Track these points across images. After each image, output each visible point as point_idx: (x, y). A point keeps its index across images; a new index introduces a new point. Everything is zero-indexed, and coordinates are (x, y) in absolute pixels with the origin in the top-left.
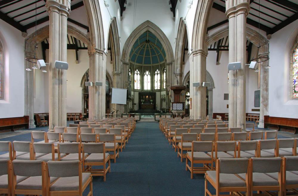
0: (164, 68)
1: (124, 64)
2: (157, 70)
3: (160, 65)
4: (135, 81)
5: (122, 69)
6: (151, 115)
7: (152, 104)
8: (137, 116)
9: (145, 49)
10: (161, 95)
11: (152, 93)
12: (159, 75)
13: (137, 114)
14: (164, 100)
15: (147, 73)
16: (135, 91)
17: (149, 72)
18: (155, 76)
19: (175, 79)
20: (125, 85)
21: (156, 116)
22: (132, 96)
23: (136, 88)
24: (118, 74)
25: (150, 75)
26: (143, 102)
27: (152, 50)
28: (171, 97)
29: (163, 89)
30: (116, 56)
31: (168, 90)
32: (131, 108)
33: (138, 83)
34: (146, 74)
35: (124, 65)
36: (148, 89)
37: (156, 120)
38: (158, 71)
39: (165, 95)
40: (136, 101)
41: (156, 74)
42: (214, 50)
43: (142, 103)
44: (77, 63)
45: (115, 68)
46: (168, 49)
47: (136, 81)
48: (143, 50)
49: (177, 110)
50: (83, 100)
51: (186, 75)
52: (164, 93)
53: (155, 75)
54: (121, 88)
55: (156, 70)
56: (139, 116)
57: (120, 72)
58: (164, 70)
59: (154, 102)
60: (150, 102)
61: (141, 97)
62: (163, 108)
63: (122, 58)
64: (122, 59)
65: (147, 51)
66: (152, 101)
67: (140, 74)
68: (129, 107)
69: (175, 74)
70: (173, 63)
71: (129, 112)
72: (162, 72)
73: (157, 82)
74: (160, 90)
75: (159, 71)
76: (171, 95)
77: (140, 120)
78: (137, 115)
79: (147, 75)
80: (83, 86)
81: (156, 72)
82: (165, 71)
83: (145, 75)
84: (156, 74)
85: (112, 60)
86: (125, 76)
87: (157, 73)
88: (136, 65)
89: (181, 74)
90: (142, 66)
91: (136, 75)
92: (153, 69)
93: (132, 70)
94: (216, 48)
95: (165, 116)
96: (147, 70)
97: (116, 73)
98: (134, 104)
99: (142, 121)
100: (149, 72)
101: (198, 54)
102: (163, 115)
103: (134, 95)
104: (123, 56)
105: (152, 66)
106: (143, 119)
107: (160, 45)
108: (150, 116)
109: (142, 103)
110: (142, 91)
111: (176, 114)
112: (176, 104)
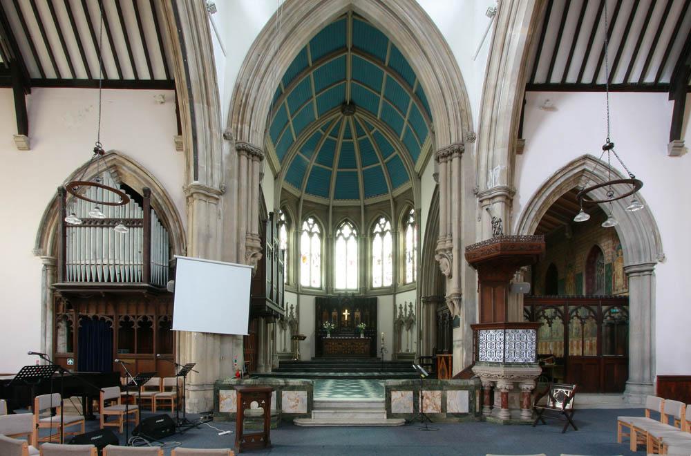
0: (409, 209)
1: (239, 150)
2: (382, 221)
3: (394, 199)
4: (304, 258)
5: (229, 175)
6: (363, 382)
7: (362, 336)
8: (292, 394)
9: (340, 141)
10: (398, 306)
11: (365, 303)
12: (388, 236)
13: (292, 382)
14: (410, 322)
15: (347, 229)
16: (300, 291)
17: (352, 229)
18: (374, 242)
19: (480, 218)
20: (243, 247)
21: (396, 395)
22: (292, 308)
23: (304, 282)
24: (208, 195)
25: (356, 238)
26: (333, 332)
27: (365, 145)
28: (460, 300)
29: (405, 284)
30: (197, 106)
31: (446, 272)
32: (289, 350)
33: (313, 267)
34: (341, 234)
35: (239, 156)
36: (385, 285)
37: (397, 416)
38: (385, 224)
39: (414, 304)
40: (307, 325)
41: (378, 235)
42: (656, 87)
43: (329, 336)
44: (20, 149)
45: (194, 167)
46: (443, 83)
47: (308, 257)
48: (330, 146)
49: (506, 364)
50: (50, 314)
51: (530, 204)
52: (409, 298)
53: (373, 235)
54: (224, 258)
55: (377, 221)
56: (303, 395)
57: (216, 187)
58: (406, 217)
59: (372, 331)
60: (358, 332)
61: (325, 314)
62: (404, 350)
63: (230, 124)
64: (231, 131)
65: (348, 149)
66: (362, 326)
67: (321, 235)
68: (278, 349)
69: (477, 194)
70: (467, 146)
71: (277, 365)
72: (400, 225)
73: (381, 261)
74: (393, 290)
75: (388, 223)
76: (460, 295)
77: (308, 415)
78: (293, 388)
79: (347, 239)
80: (48, 252)
81: (377, 229)
82: (412, 220)
83: (337, 238)
84: (378, 235)
85: (180, 132)
86: (244, 207)
87: (383, 229)
88: (304, 201)
89: (507, 189)
90: (328, 206)
91: (304, 238)
92: (365, 216)
93: (293, 220)
94: (666, 79)
95: (438, 393)
96: (346, 221)
97: (198, 187)
98: (297, 337)
99: (319, 418)
100: (354, 228)
101: (497, 199)
102: (431, 389)
103: (298, 307)
104: (235, 117)
105: (365, 206)
106: (326, 407)
107: (404, 72)
108: (362, 392)
109: (326, 333)
110: (327, 292)
111: (502, 385)
112: (501, 331)
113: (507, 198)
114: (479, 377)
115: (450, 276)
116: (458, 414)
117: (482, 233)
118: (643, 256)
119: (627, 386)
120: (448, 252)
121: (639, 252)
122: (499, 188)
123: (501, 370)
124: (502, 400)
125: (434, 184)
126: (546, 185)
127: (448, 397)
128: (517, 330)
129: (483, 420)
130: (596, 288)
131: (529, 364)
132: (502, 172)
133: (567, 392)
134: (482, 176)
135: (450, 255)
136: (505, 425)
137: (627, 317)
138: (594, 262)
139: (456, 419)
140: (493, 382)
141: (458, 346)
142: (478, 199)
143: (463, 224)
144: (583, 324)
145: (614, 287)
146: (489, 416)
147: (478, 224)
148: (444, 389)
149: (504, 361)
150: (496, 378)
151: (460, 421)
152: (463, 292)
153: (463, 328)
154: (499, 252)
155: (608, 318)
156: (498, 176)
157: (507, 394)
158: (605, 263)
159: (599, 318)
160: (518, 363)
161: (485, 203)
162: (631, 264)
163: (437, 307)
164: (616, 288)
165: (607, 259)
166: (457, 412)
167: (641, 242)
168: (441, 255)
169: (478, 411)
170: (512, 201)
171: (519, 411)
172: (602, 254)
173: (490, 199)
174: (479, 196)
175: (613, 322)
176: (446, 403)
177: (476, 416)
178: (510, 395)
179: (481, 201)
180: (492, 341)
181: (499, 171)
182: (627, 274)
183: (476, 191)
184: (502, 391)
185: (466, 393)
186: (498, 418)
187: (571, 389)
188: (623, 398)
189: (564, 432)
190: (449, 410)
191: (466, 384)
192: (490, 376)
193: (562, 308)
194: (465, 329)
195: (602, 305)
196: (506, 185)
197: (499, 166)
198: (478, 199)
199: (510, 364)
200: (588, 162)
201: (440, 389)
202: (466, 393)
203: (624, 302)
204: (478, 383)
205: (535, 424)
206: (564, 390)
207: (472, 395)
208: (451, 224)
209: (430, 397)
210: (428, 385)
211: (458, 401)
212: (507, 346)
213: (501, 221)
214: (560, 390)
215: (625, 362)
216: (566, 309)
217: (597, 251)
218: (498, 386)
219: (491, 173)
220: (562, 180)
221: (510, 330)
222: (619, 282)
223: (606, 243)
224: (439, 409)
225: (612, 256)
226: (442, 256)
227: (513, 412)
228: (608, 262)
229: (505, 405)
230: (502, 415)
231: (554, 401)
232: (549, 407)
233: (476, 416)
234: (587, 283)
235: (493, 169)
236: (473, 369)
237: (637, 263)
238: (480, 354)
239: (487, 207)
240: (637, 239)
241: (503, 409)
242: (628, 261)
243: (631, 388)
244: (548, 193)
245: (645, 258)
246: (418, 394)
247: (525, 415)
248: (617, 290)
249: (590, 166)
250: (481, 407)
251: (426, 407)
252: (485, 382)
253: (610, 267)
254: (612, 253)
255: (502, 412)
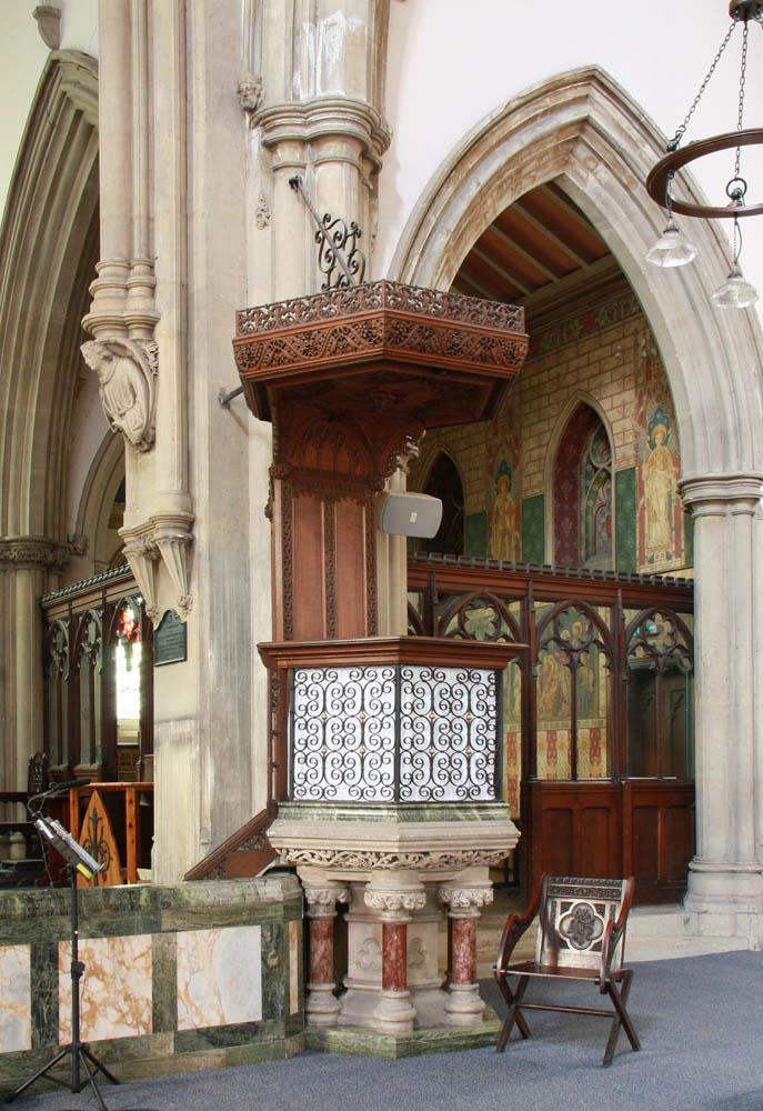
19: (265, 217)
28: (189, 544)
31: (131, 423)
69: (255, 113)
76: (189, 524)
95: (140, 944)
101: (333, 149)
111: (386, 894)
112: (382, 675)
113: (365, 155)
114: (291, 869)
115: (147, 442)
116: (223, 1029)
117: (277, 269)
118: (733, 456)
119: (692, 877)
120: (137, 334)
121: (723, 435)
122: (340, 107)
123: (387, 834)
124: (386, 957)
125: (40, 56)
126: (476, 147)
127: (183, 961)
128: (439, 671)
129: (314, 1046)
130: (583, 553)
131: (481, 806)
132: (350, 39)
133: (601, 909)
134: (276, 40)
135: (148, 348)
136: (401, 1056)
137: (689, 650)
138: (576, 460)
139: (213, 1056)
140: (348, 885)
141: (180, 742)
142: (256, 137)
143: (198, 227)
144: (573, 666)
145: (642, 552)
146: (335, 1026)
147: (257, 237)
148: (166, 923)
149: (397, 795)
150: (365, 867)
151: (229, 1063)
152: (201, 512)
153: (202, 657)
154: (377, 349)
155: (640, 652)
156: (335, 56)
157: (402, 928)
158: (613, 470)
159: (615, 646)
160: (444, 806)
161: (286, 154)
162: (702, 473)
163: (45, 589)
164: (648, 555)
165: (622, 452)
166: (216, 1022)
167: (727, 398)
168: (106, 345)
169: (294, 1008)
170: (376, 169)
171: (437, 996)
172: (603, 436)
173: (304, 142)
174: (264, 122)
175: (652, 665)
176: (173, 987)
177: (289, 1034)
178: (411, 933)
179: (271, 146)
180: (348, 707)
181: (337, 36)
182: (689, 508)
183: (253, 99)
184: (388, 917)
185: (250, 939)
186: (374, 1032)
187: (615, 895)
188: (687, 921)
189: (607, 1062)
190: (188, 1019)
191: (250, 900)
192: (337, 860)
193: (515, 607)
194: (212, 665)
195: (626, 606)
196: (364, 99)
197: (338, 17)
198: (256, 137)
199: (417, 807)
200: (598, 96)
201: (153, 927)
202: (250, 939)
203: (677, 599)
204: (295, 890)
205: (503, 1042)
206: (591, 903)
207: (274, 943)
208: (149, 220)
209: (108, 967)
210: (96, 910)
211: (222, 976)
212: (406, 734)
213: (357, 233)
214: (576, 901)
215: (683, 798)
216: (527, 612)
217: (587, 425)
218: (372, 900)
219: (307, 39)
220: (526, 137)
221: (417, 671)
222: (657, 531)
223: (617, 400)
224: (147, 1016)
225: (636, 448)
226: (115, 351)
227: (421, 999)
228: (624, 466)
229: (396, 977)
230: (387, 1016)
231: (557, 944)
232: (541, 969)
233: (289, 1034)
234: (558, 533)
235: (315, 20)
236: (269, 833)
237: (717, 472)
238: (299, 768)
239: (292, 174)
240: (719, 393)
241: (392, 993)
242: (693, 466)
243: (706, 884)
244: (484, 175)
245: (740, 456)
246: (54, 959)
247: (465, 1008)
248: (651, 561)
249: (601, 112)
250: (305, 993)
251: (92, 1016)
252: (320, 887)
253: (630, 482)
254: (636, 435)
255: (382, 1005)
